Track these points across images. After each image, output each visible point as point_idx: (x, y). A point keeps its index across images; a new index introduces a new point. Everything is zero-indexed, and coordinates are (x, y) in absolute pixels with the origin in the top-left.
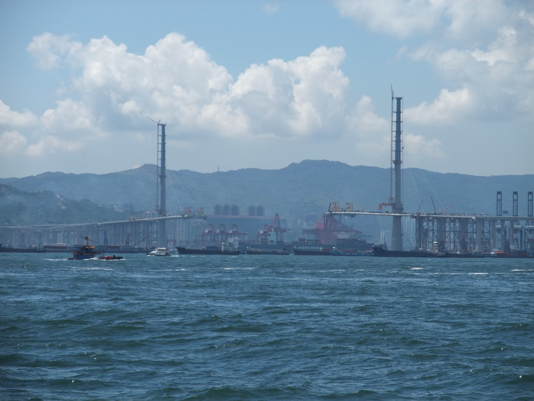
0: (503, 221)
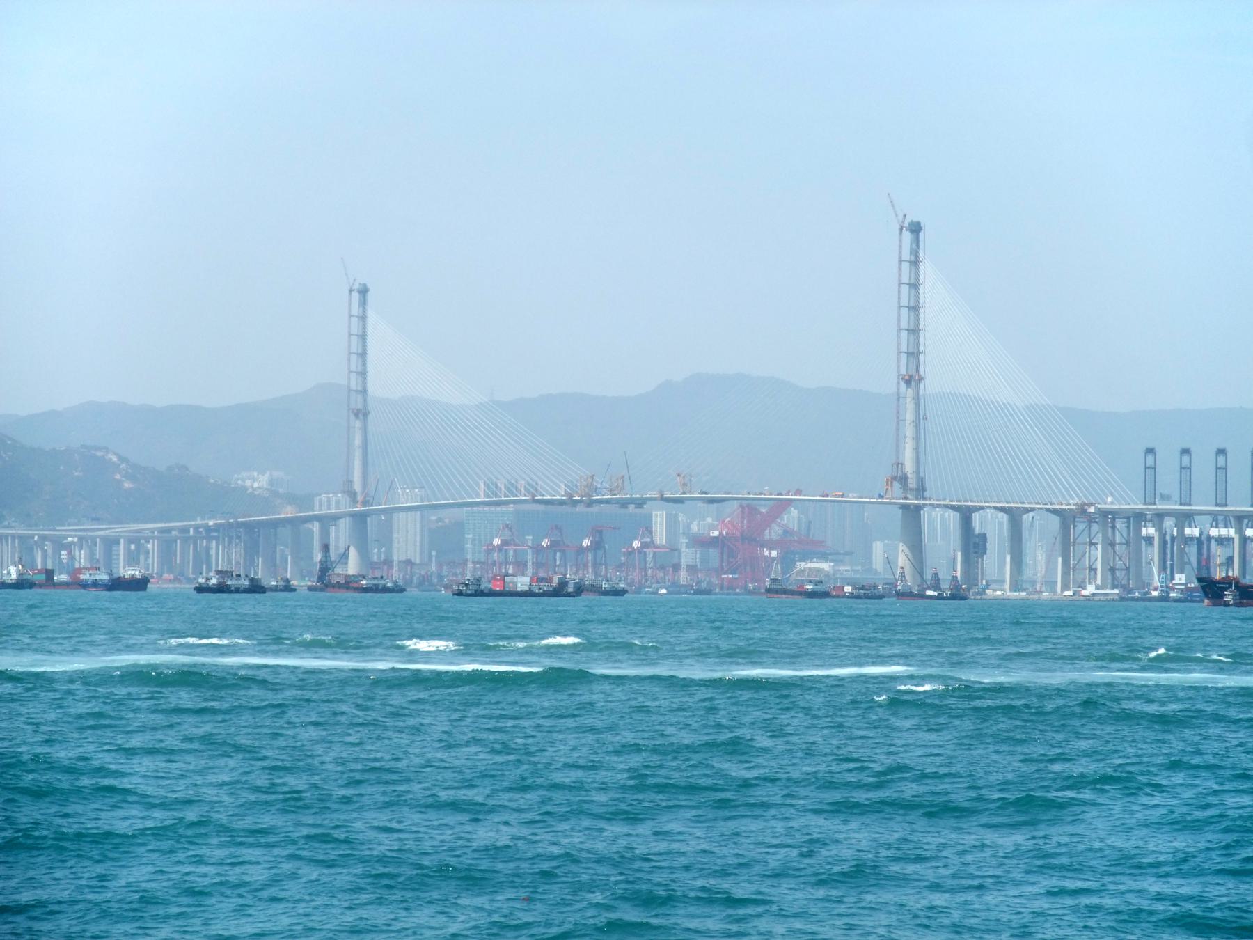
0: (1160, 516)
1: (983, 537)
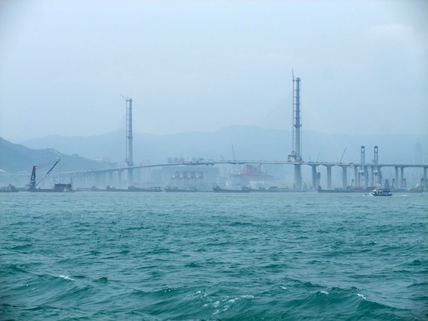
1: (319, 174)
